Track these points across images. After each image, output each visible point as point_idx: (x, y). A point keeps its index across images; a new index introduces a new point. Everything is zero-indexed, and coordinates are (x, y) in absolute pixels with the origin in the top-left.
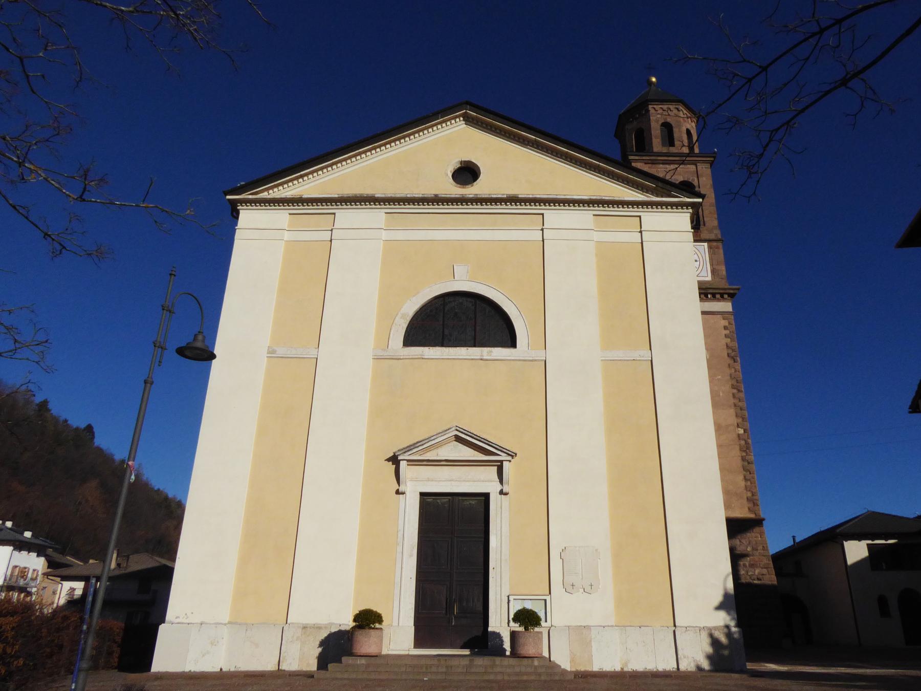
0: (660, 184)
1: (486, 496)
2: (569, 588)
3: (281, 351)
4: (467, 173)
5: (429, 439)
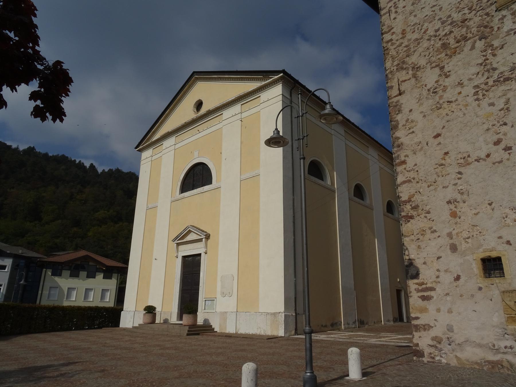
0: (265, 74)
1: (200, 255)
2: (224, 295)
3: (150, 206)
4: (199, 105)
5: (181, 233)
